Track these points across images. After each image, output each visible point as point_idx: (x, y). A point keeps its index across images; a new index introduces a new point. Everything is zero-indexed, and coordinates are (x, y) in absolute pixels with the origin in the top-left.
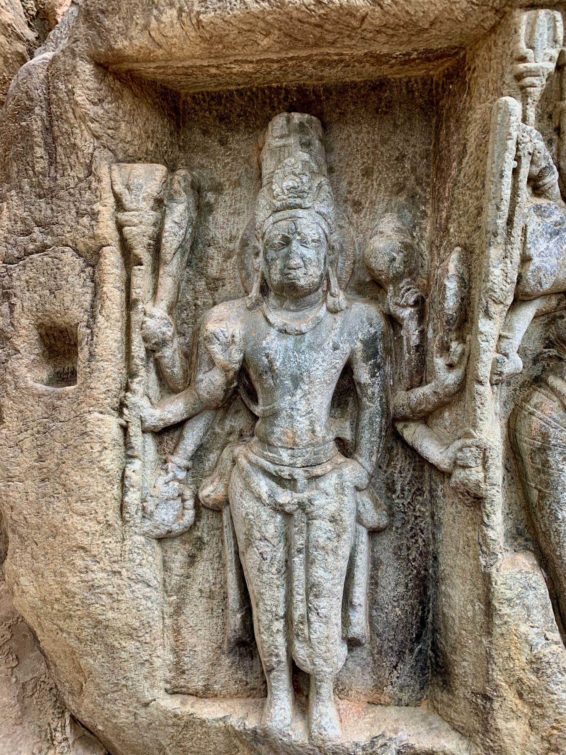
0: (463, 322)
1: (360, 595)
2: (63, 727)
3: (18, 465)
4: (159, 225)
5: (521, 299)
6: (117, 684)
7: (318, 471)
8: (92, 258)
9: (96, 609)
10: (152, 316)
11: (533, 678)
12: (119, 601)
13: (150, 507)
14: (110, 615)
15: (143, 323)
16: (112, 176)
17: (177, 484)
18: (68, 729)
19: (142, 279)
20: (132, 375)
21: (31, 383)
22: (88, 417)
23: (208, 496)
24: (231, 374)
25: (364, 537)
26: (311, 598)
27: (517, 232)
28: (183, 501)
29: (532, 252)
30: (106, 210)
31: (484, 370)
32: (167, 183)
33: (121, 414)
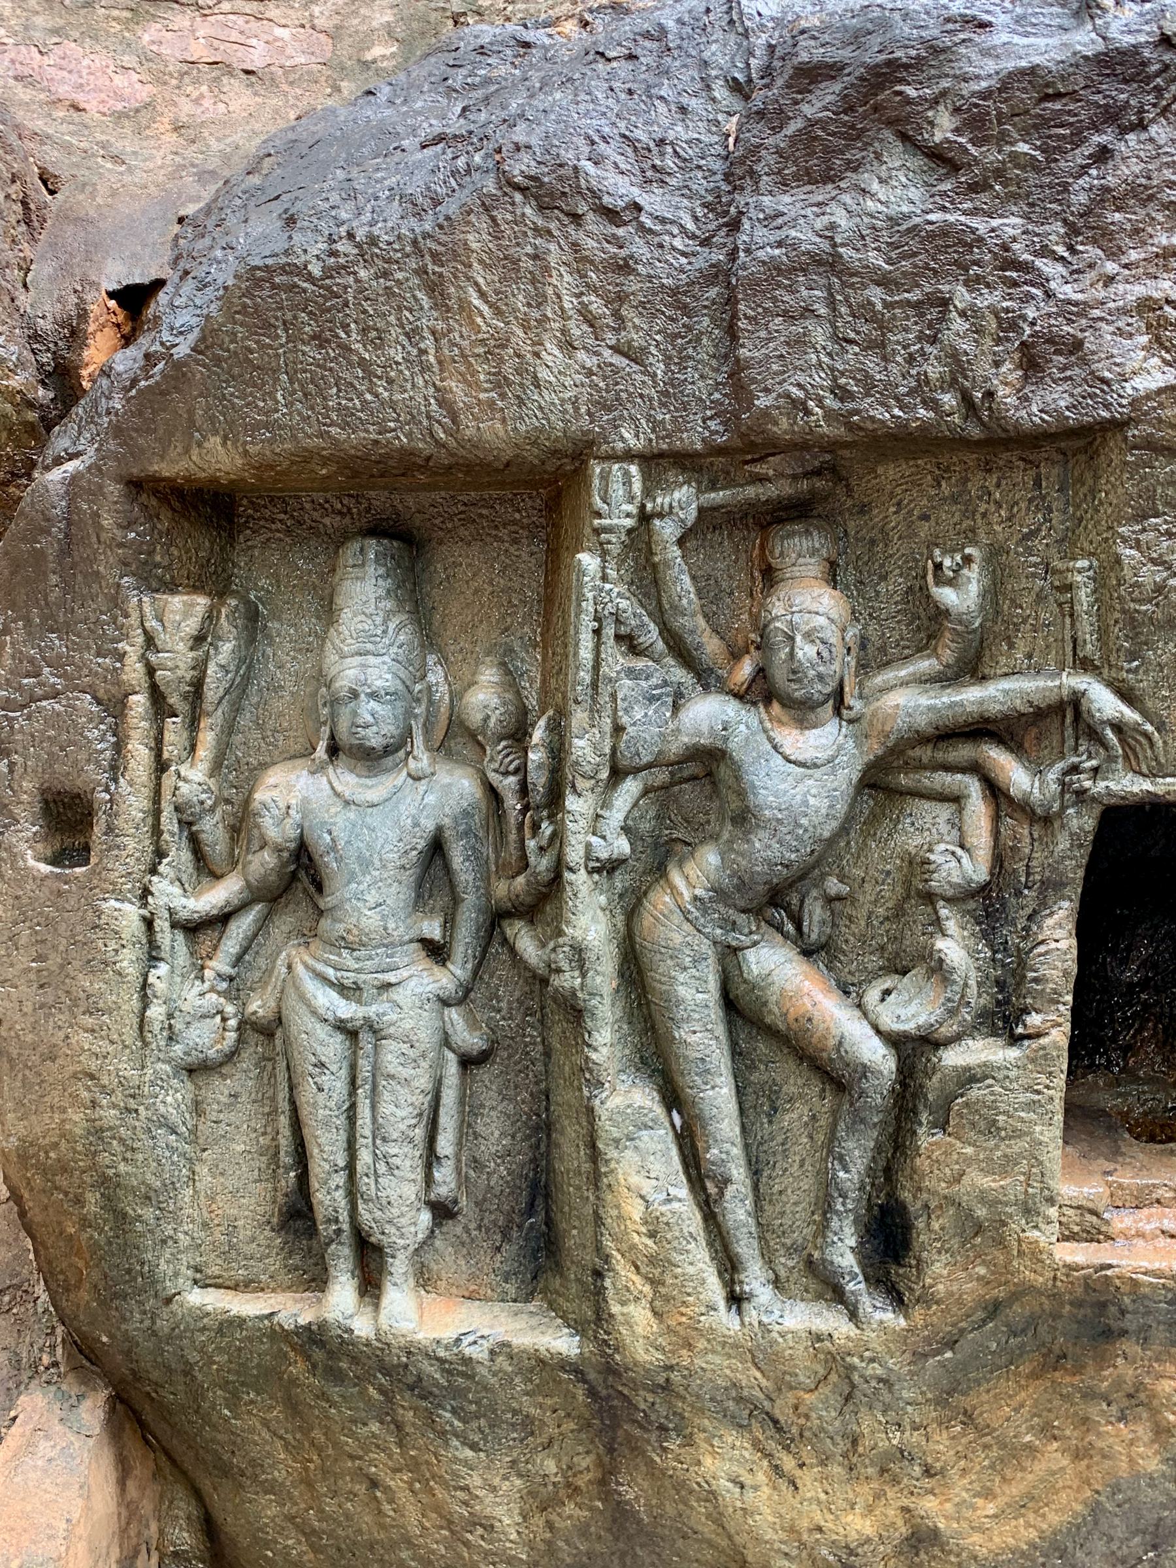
0: (555, 799)
1: (445, 1144)
2: (53, 1347)
3: (12, 965)
4: (201, 667)
5: (618, 774)
6: (129, 1272)
7: (391, 977)
8: (115, 707)
9: (105, 1158)
10: (185, 780)
11: (650, 1242)
12: (133, 1150)
13: (178, 1025)
14: (122, 1168)
15: (176, 788)
16: (142, 605)
17: (214, 996)
18: (59, 1351)
19: (174, 731)
20: (160, 854)
21: (31, 862)
22: (104, 905)
23: (255, 1013)
24: (286, 854)
25: (452, 1068)
26: (378, 1142)
27: (604, 698)
28: (224, 1020)
29: (625, 720)
30: (132, 649)
31: (574, 854)
32: (211, 616)
33: (145, 905)
